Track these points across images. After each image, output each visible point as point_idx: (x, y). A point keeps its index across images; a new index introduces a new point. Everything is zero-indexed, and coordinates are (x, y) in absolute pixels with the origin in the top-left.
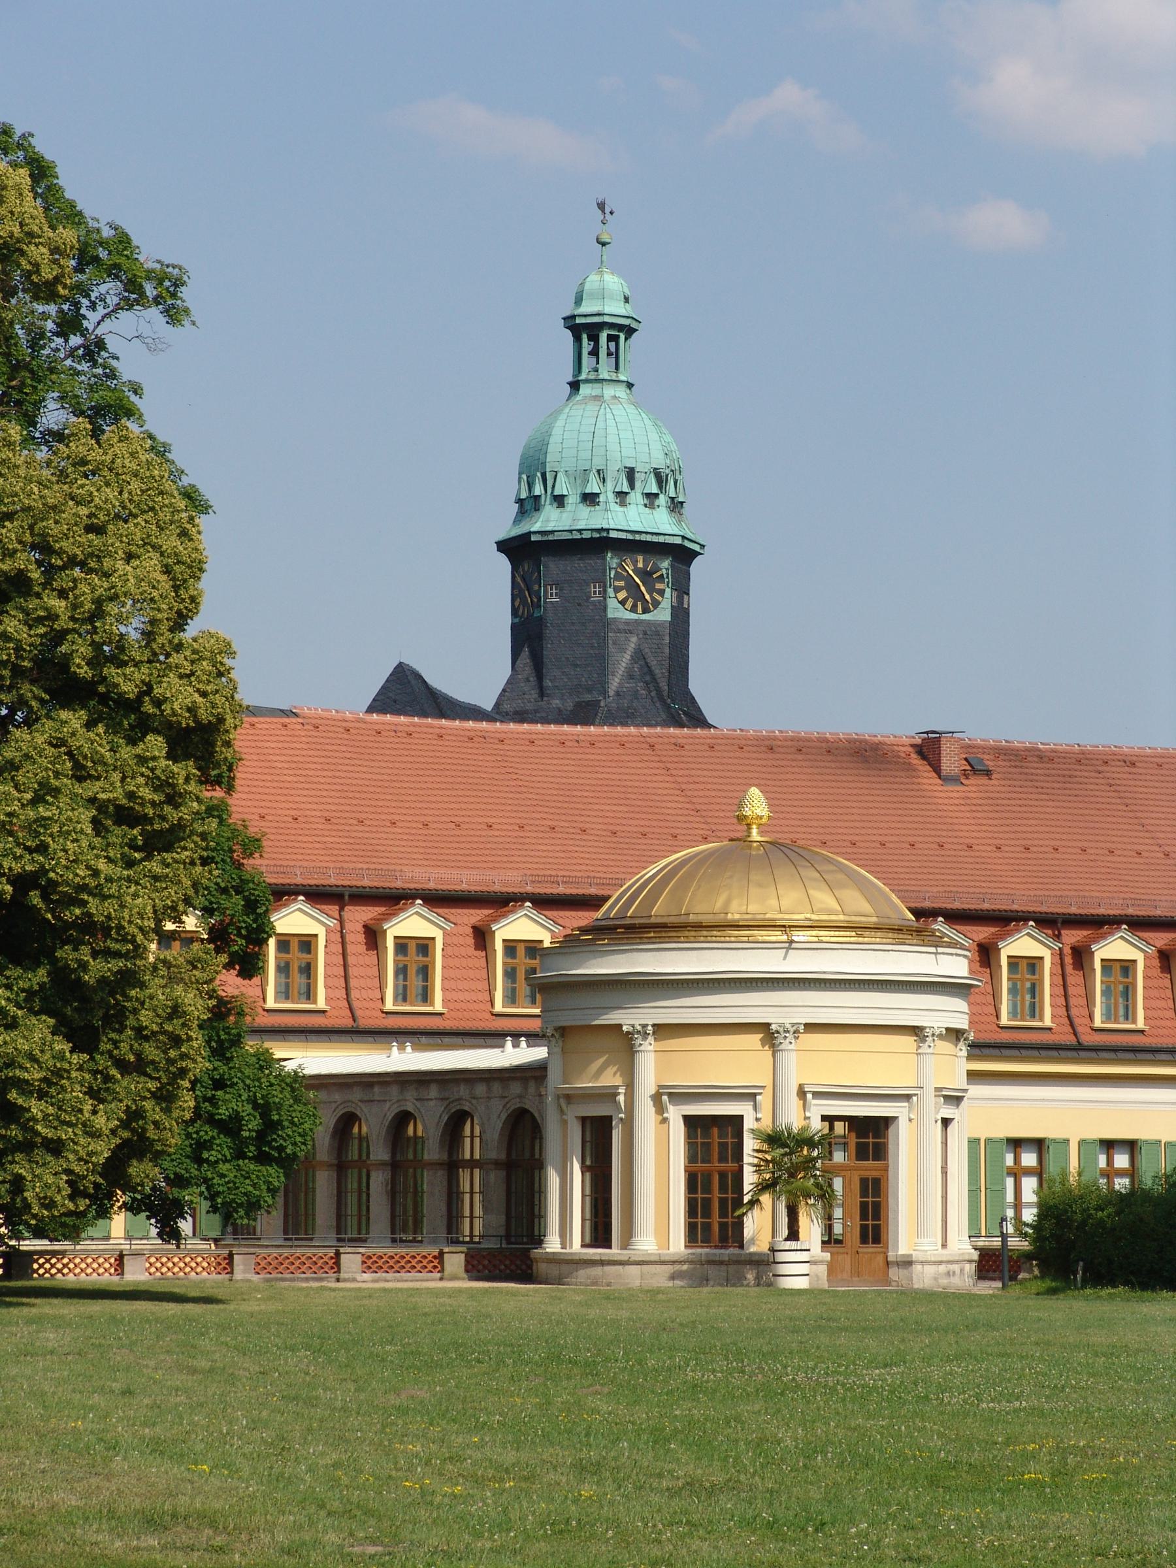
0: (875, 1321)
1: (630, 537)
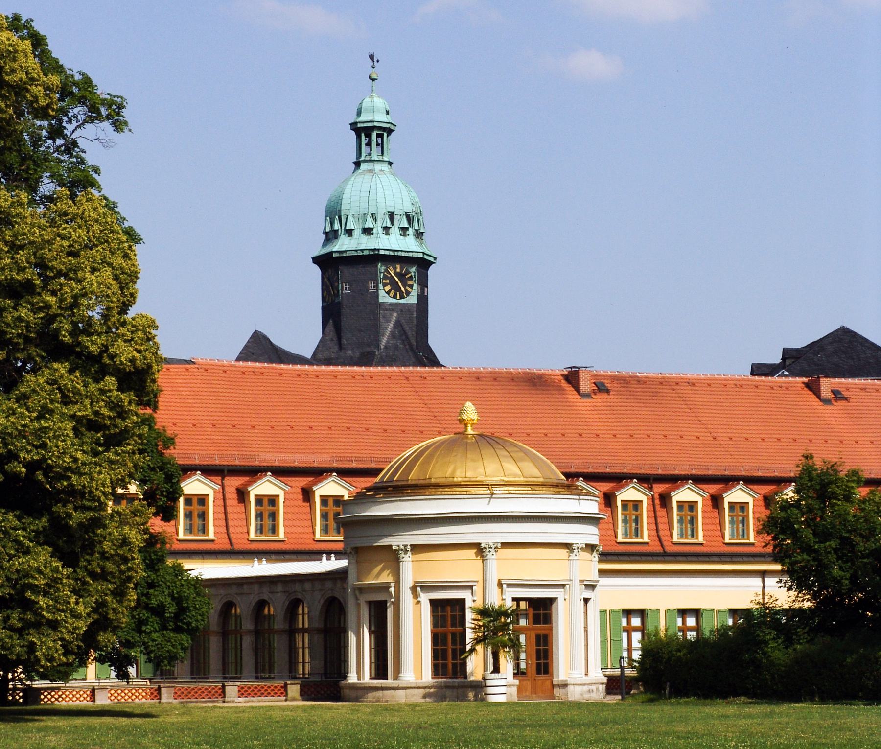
1: (392, 253)
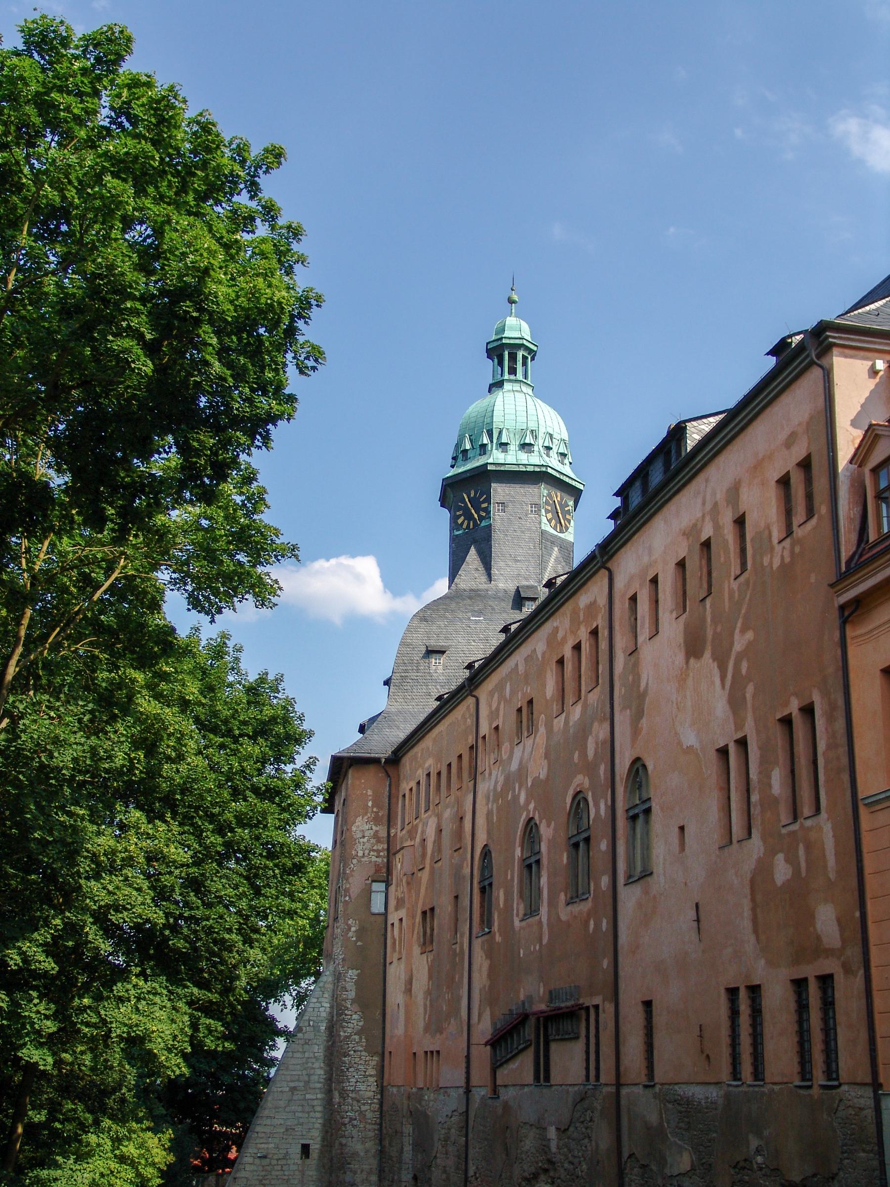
0: (222, 746)
1: (558, 475)
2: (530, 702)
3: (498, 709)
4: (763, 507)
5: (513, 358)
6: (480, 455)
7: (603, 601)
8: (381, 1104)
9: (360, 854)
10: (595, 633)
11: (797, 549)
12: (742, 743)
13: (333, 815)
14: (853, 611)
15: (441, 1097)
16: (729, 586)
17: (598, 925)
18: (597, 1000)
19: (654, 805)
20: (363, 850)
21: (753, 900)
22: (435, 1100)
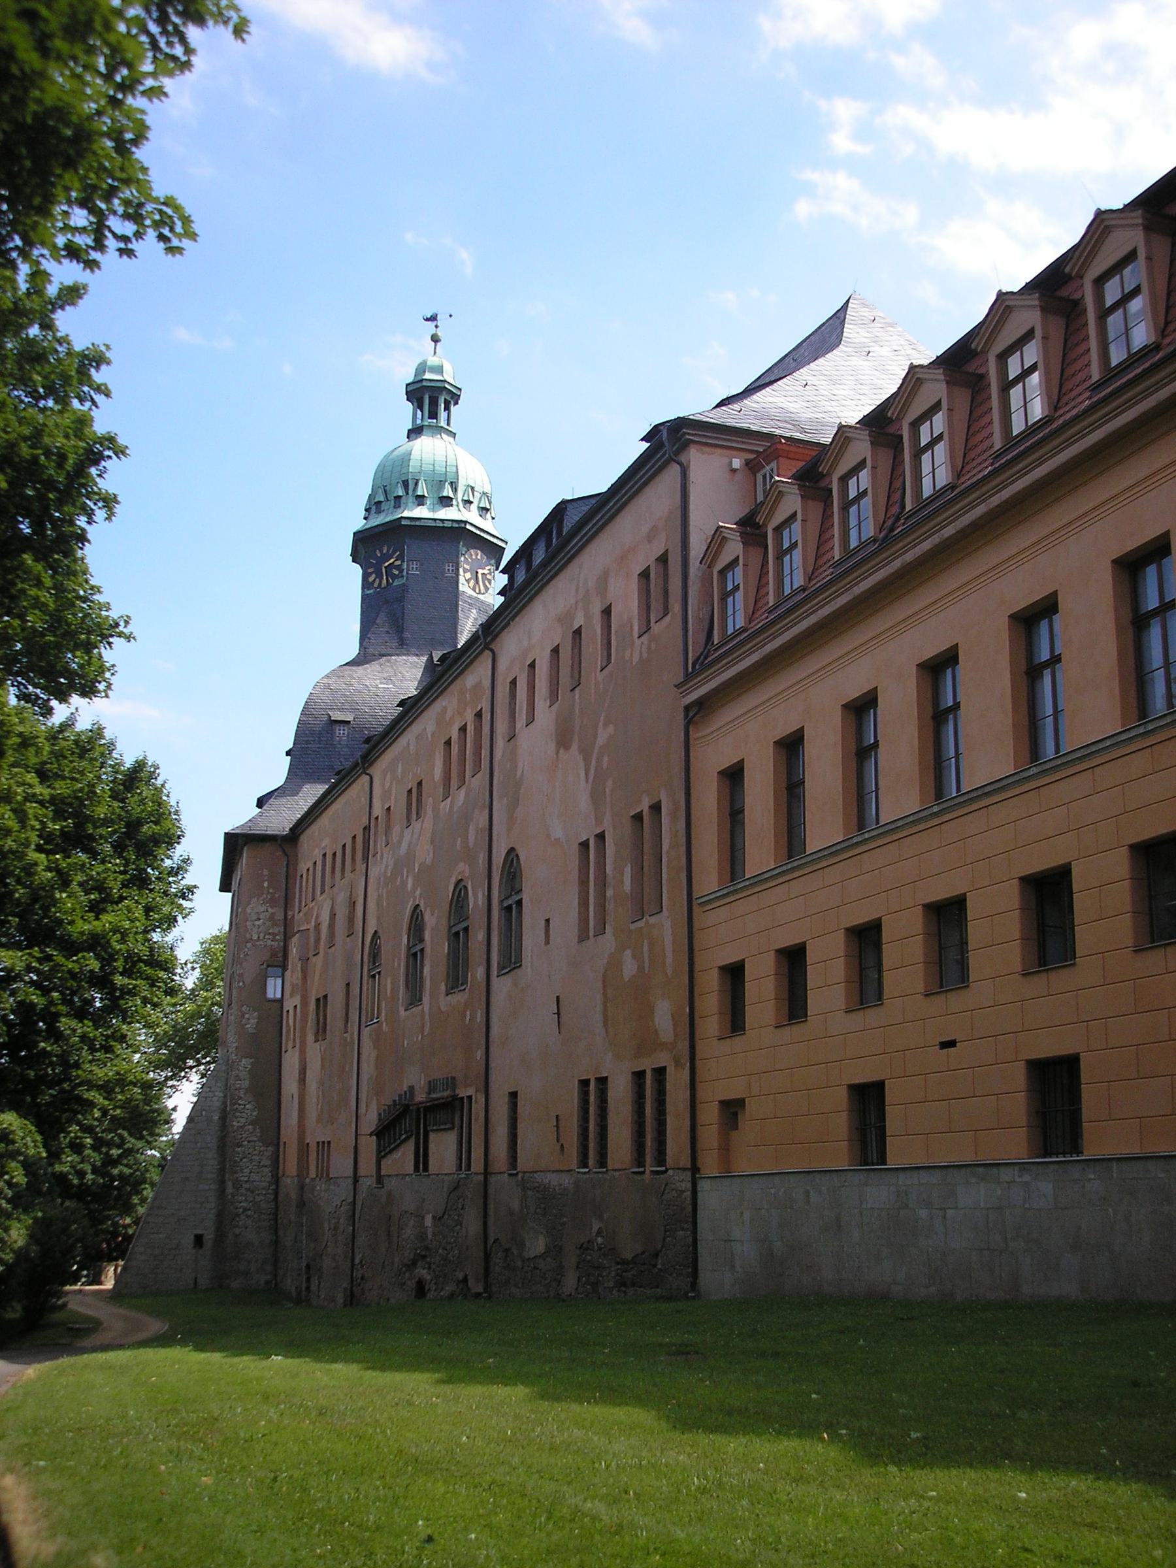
1: (478, 532)
2: (420, 784)
3: (390, 788)
4: (626, 600)
5: (434, 403)
6: (395, 507)
7: (487, 683)
8: (276, 1194)
9: (255, 937)
10: (479, 715)
11: (653, 646)
12: (601, 837)
13: (230, 895)
14: (698, 712)
15: (332, 1187)
16: (594, 677)
17: (473, 1017)
18: (470, 1091)
19: (524, 897)
20: (259, 933)
21: (605, 994)
22: (326, 1191)
